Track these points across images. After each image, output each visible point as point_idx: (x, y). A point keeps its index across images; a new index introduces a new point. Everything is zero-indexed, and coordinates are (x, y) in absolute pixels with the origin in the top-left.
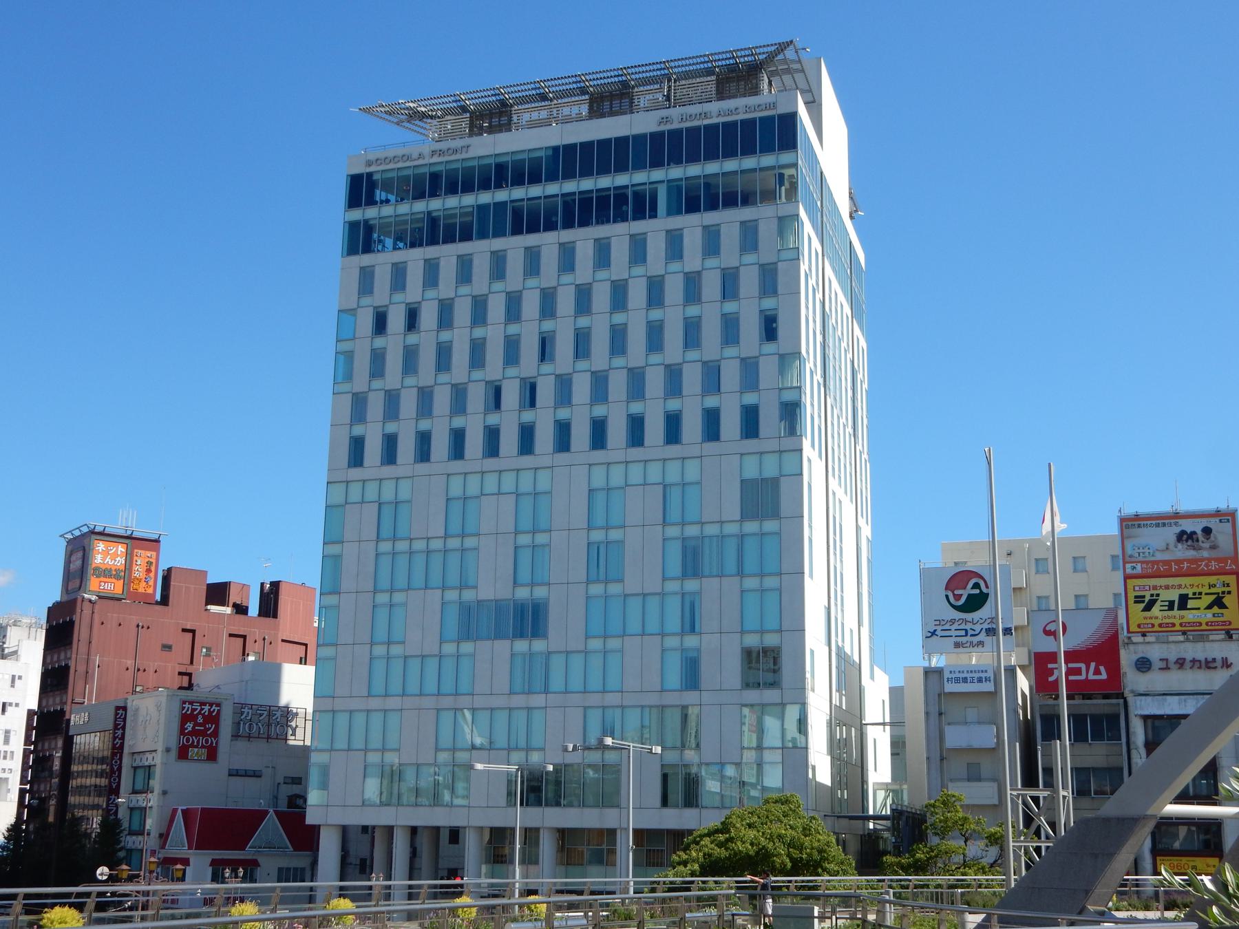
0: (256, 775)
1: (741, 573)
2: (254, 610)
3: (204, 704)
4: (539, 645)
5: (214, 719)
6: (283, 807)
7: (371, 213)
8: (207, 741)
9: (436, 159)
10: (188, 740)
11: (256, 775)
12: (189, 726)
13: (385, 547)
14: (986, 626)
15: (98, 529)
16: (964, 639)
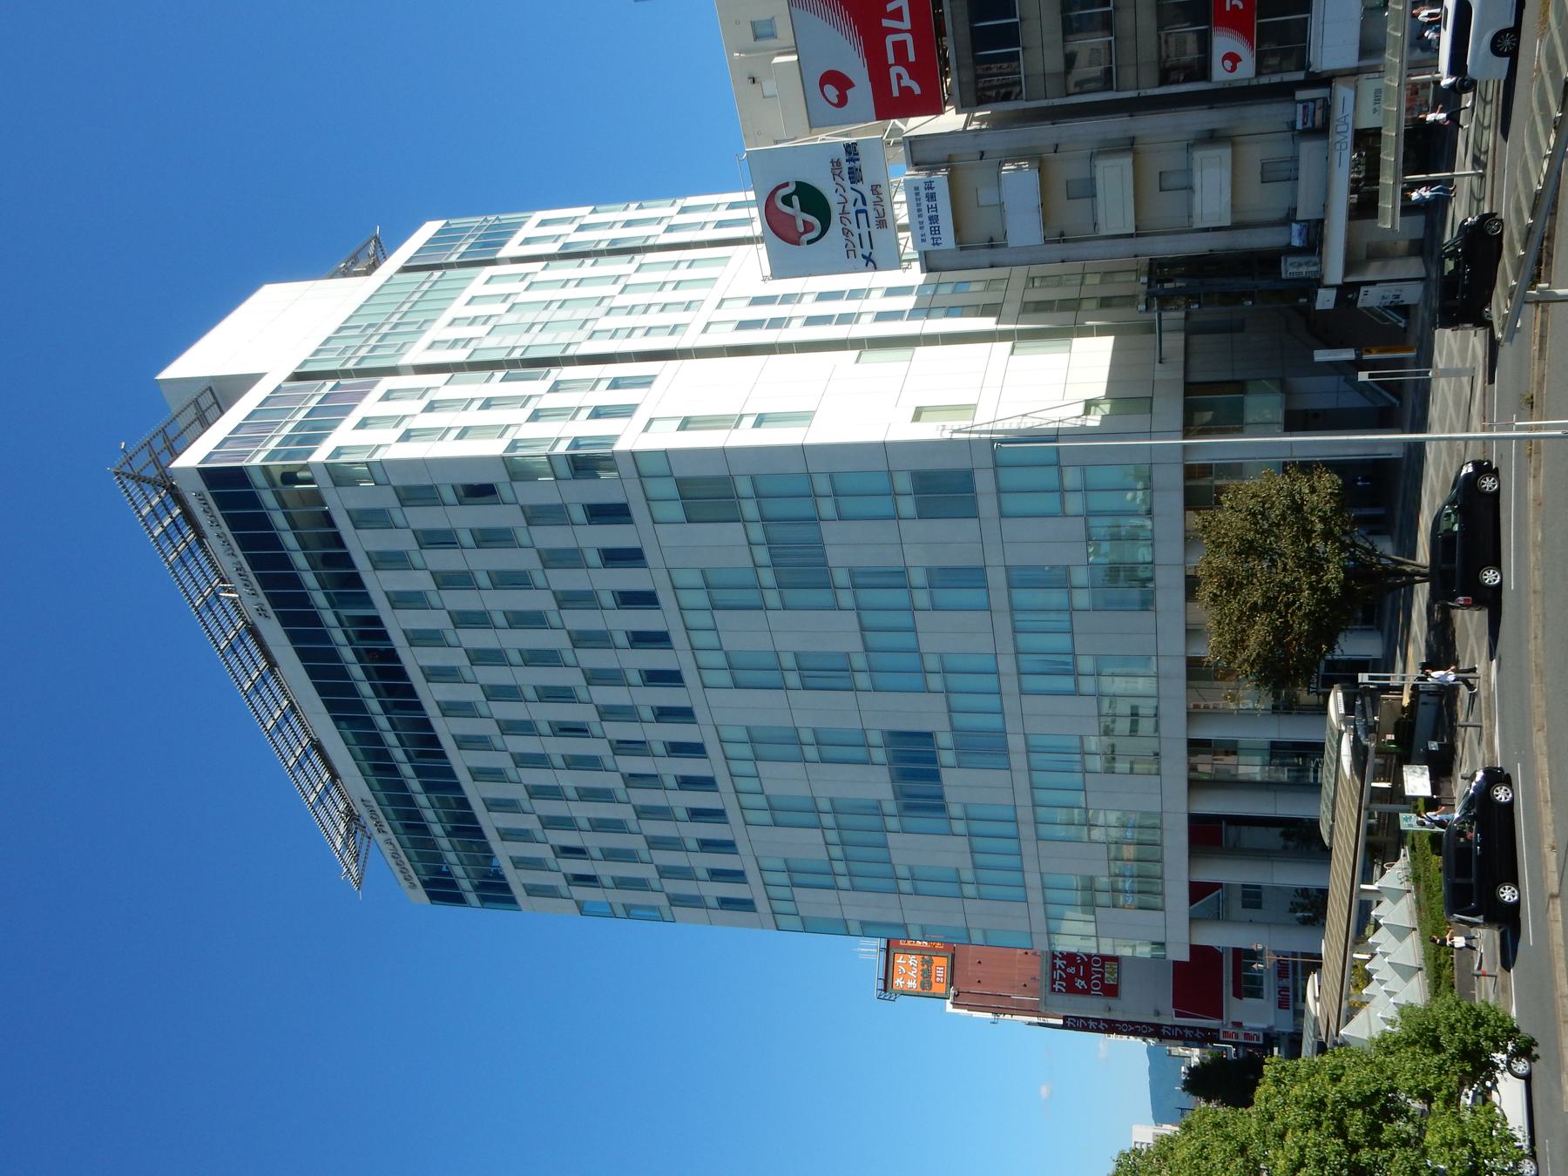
1: (816, 520)
3: (1054, 965)
4: (944, 739)
9: (387, 828)
12: (1080, 983)
13: (843, 882)
14: (847, 183)
15: (881, 986)
16: (872, 215)
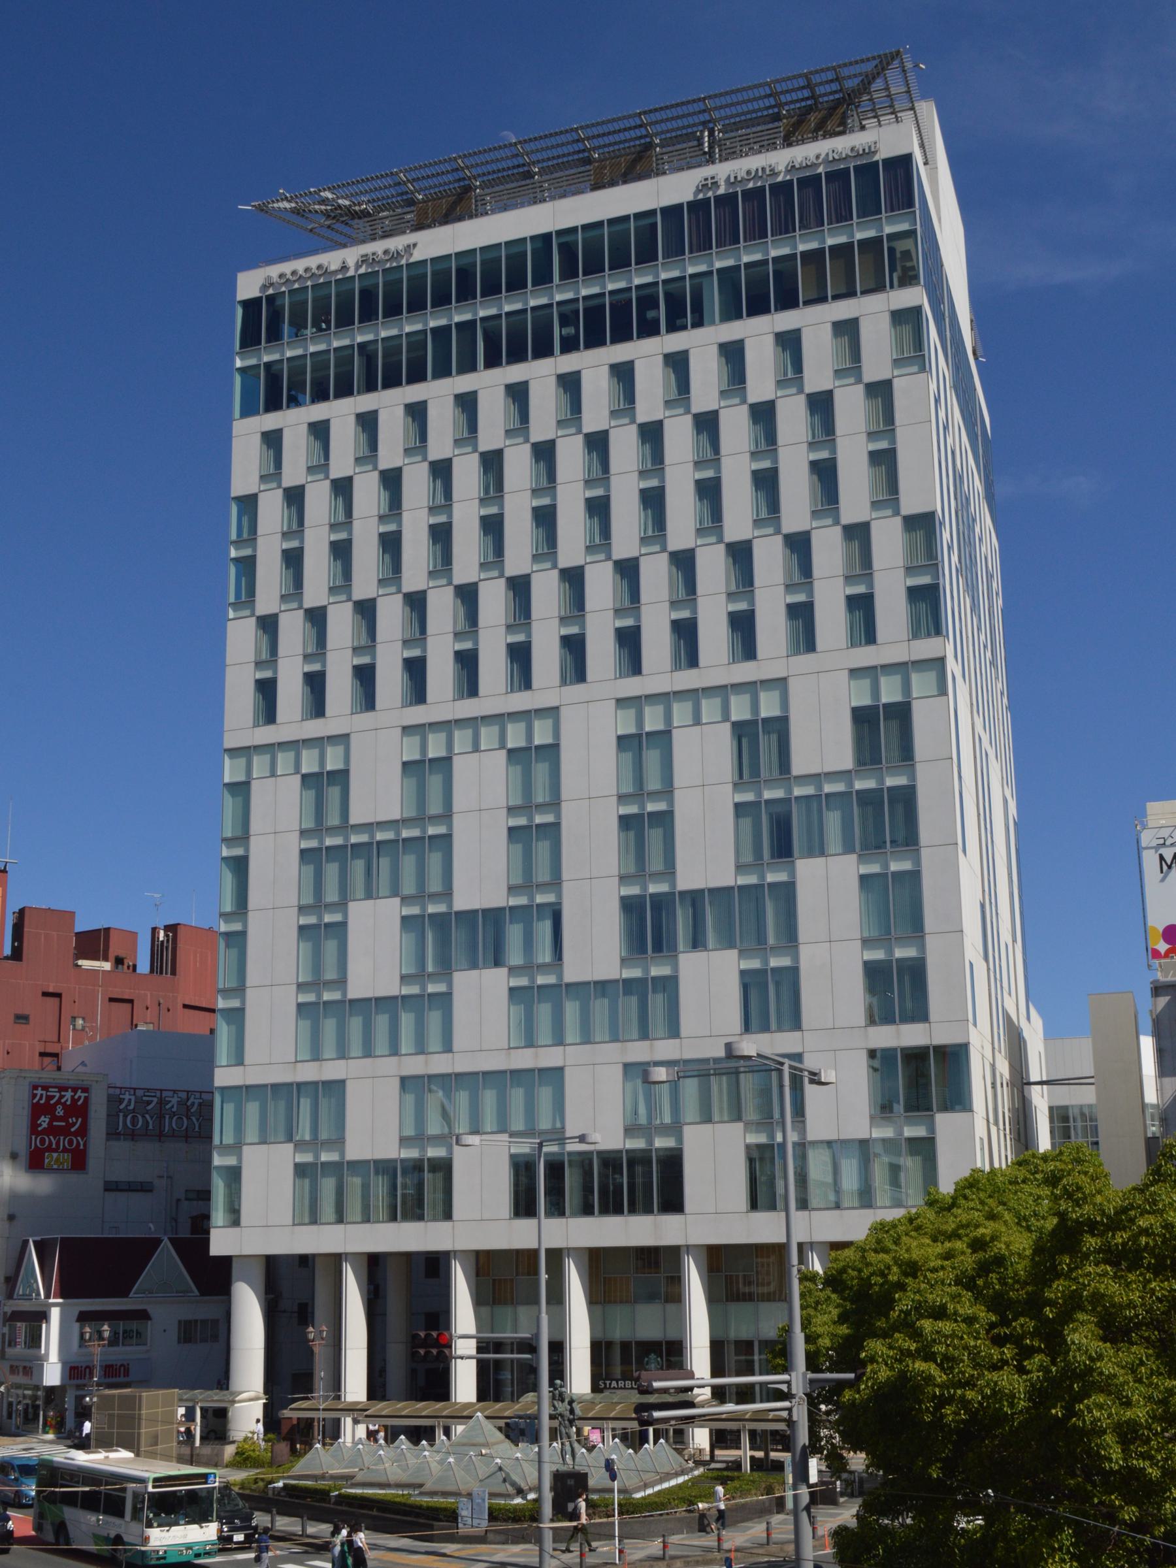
0: (144, 1188)
2: (144, 966)
5: (80, 1110)
6: (185, 1233)
7: (546, 1424)
8: (71, 1142)
10: (43, 1141)
11: (144, 1188)
12: (44, 1121)
